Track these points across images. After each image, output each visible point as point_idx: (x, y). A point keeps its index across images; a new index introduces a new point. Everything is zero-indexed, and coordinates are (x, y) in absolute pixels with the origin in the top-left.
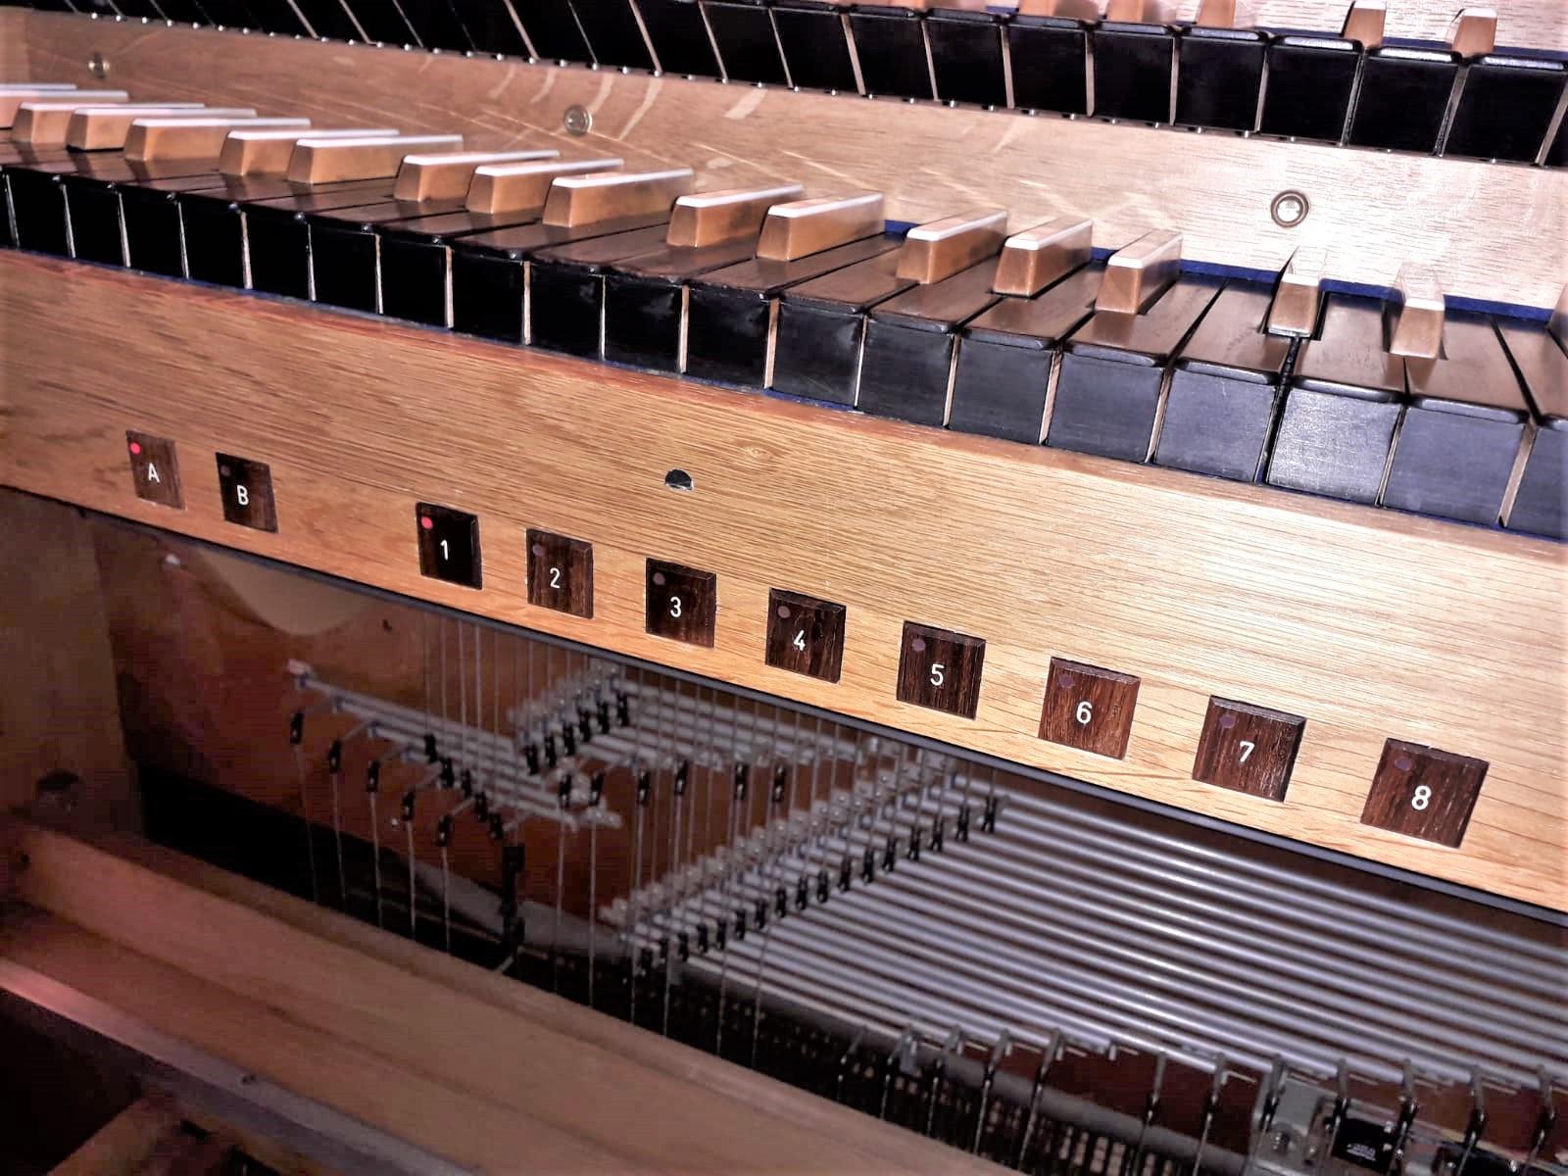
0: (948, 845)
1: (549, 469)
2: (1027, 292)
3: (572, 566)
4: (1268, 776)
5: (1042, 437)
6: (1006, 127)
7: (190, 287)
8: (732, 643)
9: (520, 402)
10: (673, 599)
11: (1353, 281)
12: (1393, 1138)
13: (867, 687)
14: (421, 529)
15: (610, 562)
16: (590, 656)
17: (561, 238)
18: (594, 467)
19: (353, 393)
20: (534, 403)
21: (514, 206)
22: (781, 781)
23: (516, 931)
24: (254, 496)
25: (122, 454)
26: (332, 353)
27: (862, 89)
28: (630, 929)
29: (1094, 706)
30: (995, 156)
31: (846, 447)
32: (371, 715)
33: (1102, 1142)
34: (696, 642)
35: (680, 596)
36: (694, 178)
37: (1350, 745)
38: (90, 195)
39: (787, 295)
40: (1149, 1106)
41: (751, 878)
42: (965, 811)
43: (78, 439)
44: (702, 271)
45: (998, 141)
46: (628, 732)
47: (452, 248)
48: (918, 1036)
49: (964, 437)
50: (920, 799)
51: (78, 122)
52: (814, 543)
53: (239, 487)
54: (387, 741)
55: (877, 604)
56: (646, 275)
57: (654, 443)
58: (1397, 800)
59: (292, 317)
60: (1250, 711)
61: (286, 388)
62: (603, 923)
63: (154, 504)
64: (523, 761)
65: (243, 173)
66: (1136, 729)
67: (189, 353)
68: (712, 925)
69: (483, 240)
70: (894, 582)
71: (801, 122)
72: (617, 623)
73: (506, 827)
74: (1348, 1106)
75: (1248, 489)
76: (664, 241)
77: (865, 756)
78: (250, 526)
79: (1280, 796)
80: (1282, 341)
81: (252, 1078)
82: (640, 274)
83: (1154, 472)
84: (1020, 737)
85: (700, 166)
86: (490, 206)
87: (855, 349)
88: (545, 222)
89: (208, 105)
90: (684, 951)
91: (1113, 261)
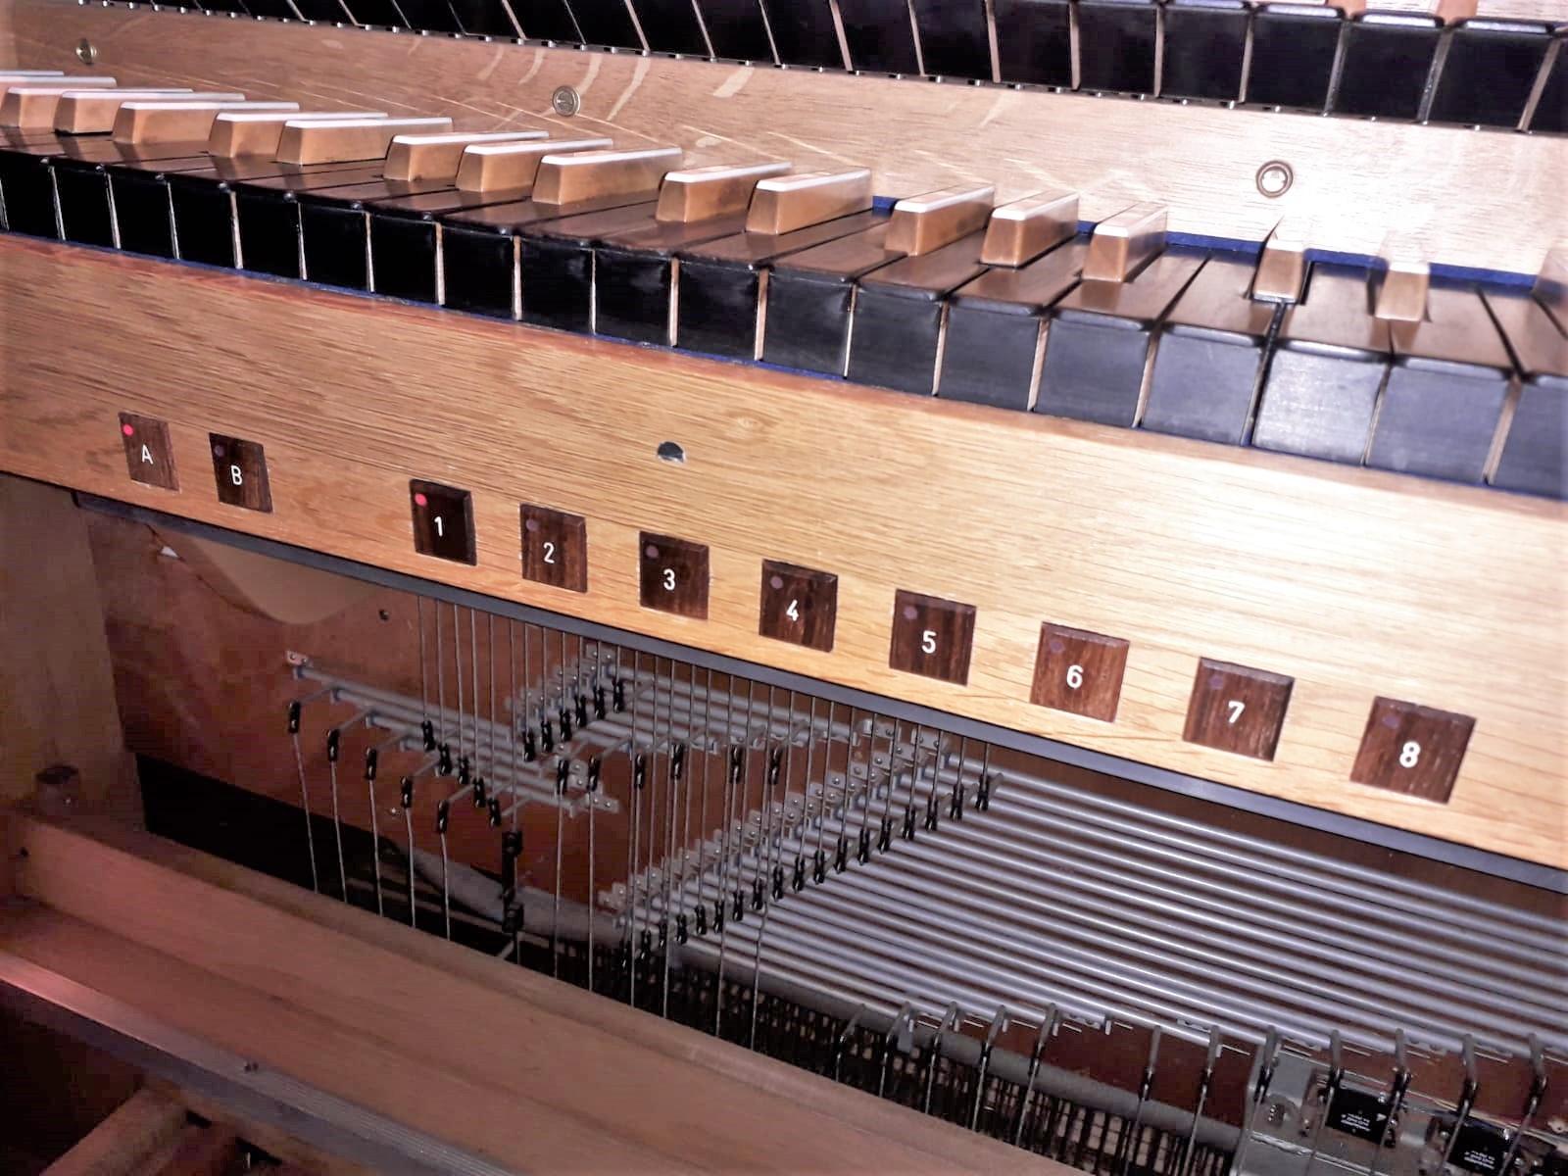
0: (942, 825)
1: (543, 443)
2: (1015, 262)
3: (565, 539)
4: (1257, 736)
5: (1031, 404)
6: (993, 102)
7: (180, 267)
8: (726, 615)
9: (509, 375)
10: (666, 572)
11: (1338, 251)
12: (1386, 1108)
13: (859, 657)
14: (415, 507)
15: (603, 536)
16: (589, 640)
17: (552, 215)
18: (586, 441)
19: (345, 370)
20: (527, 378)
21: (505, 184)
22: (775, 763)
23: (516, 920)
24: (248, 476)
25: (115, 436)
26: (323, 331)
27: (849, 66)
28: (630, 914)
29: (1085, 669)
30: (981, 130)
31: (836, 416)
32: (368, 704)
33: (1099, 1119)
34: (690, 614)
35: (673, 569)
36: (684, 157)
37: (1337, 704)
38: (81, 180)
39: (776, 265)
40: (1145, 1080)
41: (749, 860)
42: (958, 789)
43: (70, 422)
44: (690, 244)
45: (984, 117)
46: (625, 718)
47: (442, 224)
48: (915, 1014)
49: (953, 405)
50: (914, 779)
51: (66, 106)
52: (807, 513)
53: (233, 467)
54: (387, 730)
55: (869, 573)
56: (636, 248)
57: (646, 416)
58: (1386, 758)
59: (283, 295)
60: (1238, 672)
61: (278, 366)
62: (601, 908)
63: (148, 486)
64: (521, 748)
65: (232, 155)
66: (1126, 691)
67: (181, 333)
68: (710, 907)
69: (473, 217)
70: (883, 550)
71: (788, 99)
72: (612, 597)
73: (505, 814)
74: (1341, 1076)
75: (1238, 451)
76: (653, 217)
77: (858, 737)
78: (246, 507)
79: (1270, 754)
80: (1266, 306)
81: (256, 1066)
82: (629, 247)
83: (1142, 436)
84: (1011, 703)
85: (688, 145)
86: (479, 184)
87: (845, 318)
88: (535, 200)
89: (195, 90)
90: (683, 933)
91: (1098, 231)
